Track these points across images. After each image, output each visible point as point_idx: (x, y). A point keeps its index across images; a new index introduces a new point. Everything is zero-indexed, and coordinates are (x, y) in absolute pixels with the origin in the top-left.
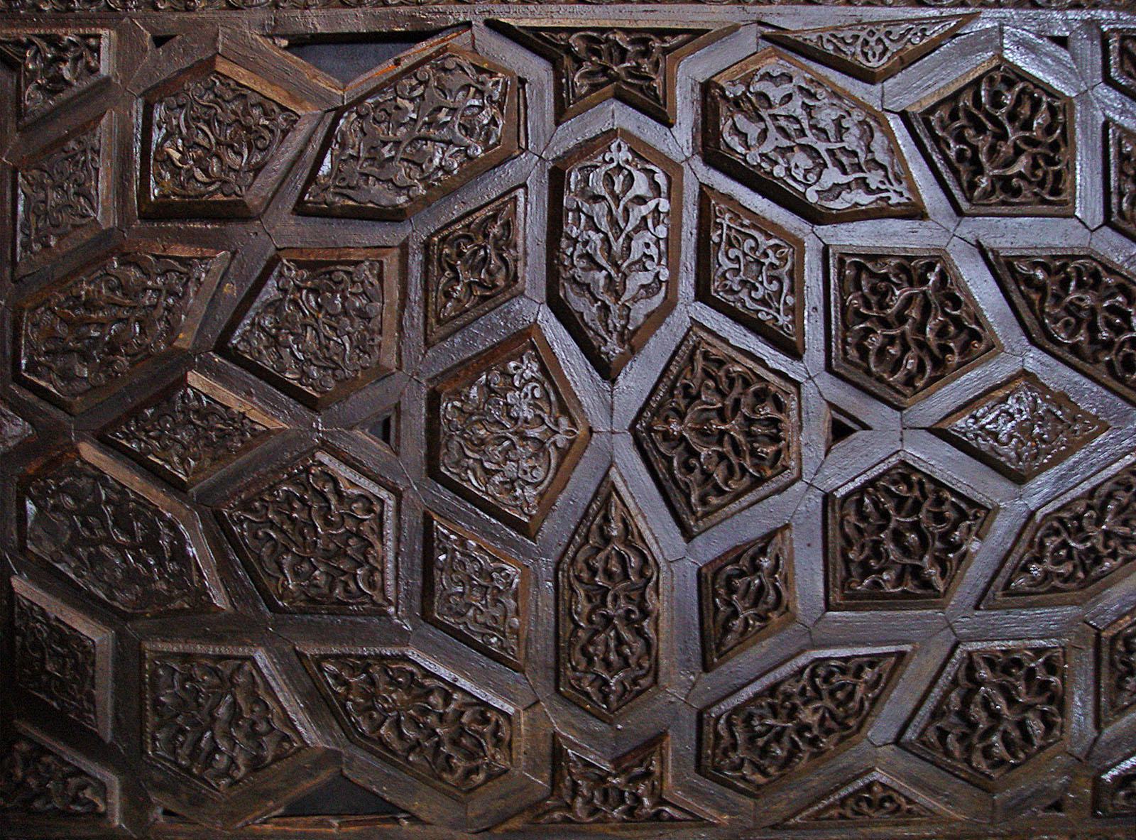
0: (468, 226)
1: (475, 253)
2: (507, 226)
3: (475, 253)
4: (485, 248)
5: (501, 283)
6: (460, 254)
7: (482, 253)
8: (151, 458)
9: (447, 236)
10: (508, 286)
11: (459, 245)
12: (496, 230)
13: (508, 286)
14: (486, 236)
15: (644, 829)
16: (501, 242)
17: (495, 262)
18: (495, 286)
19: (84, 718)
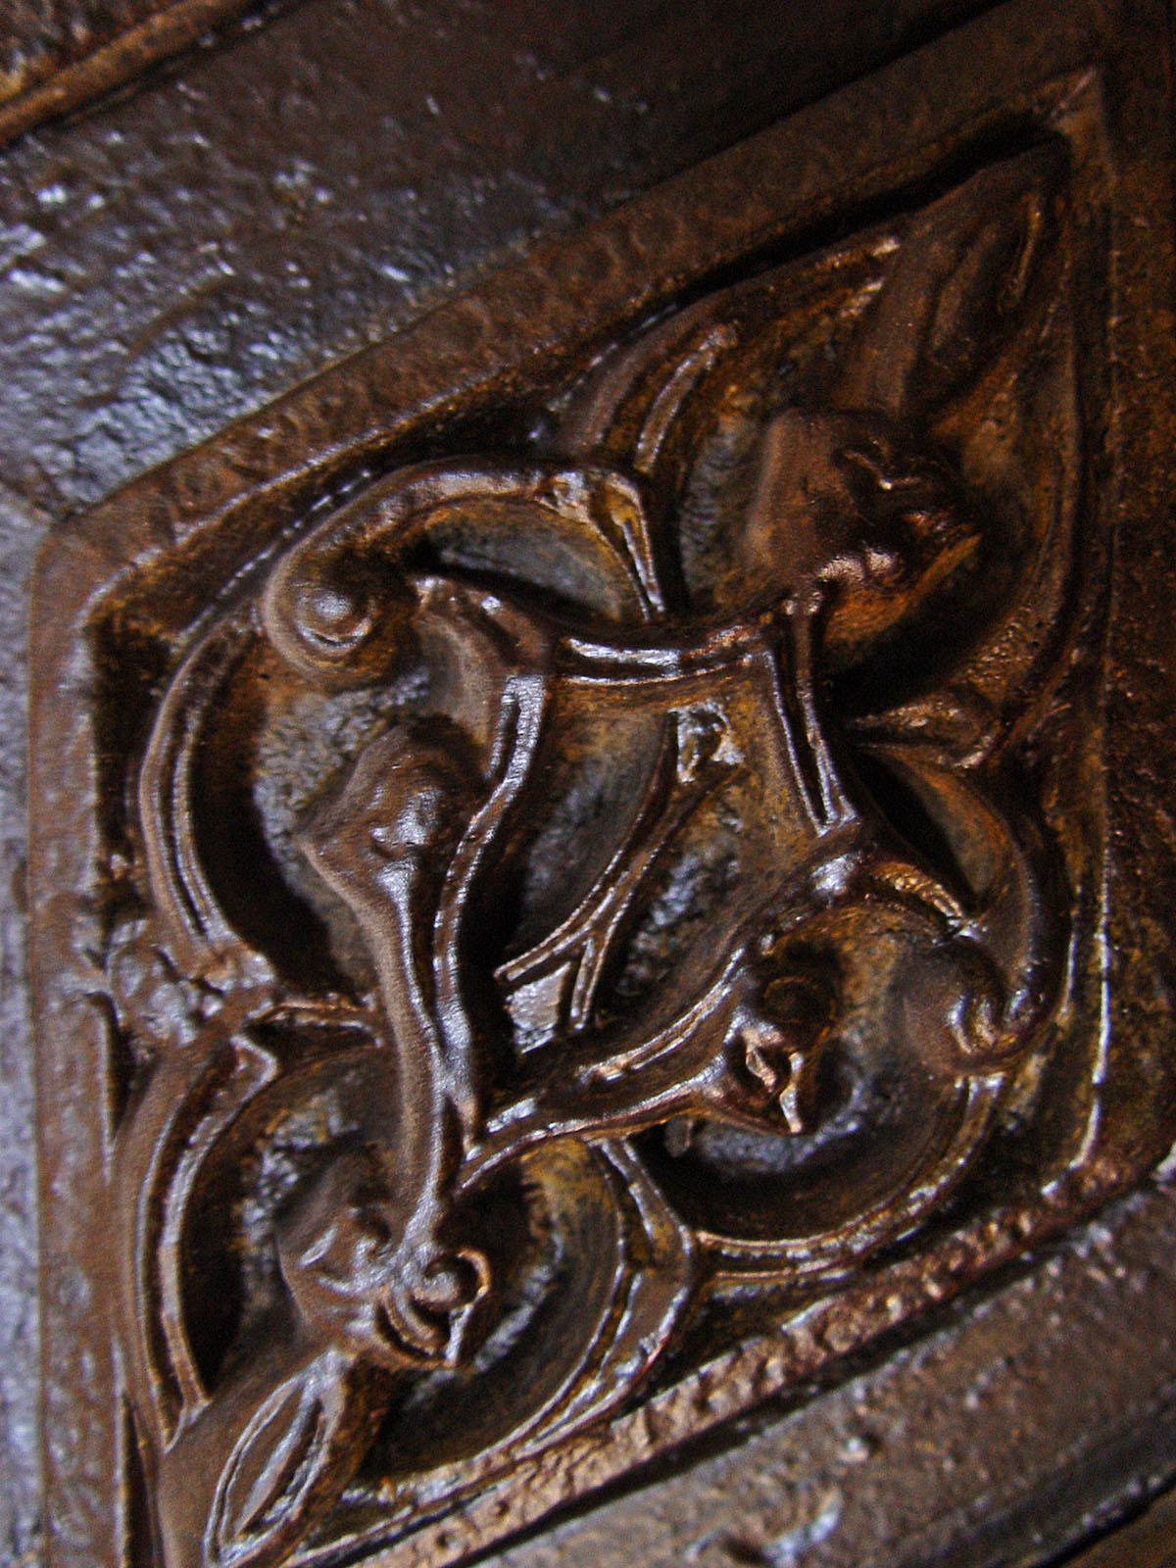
0: (706, 1333)
1: (625, 1001)
2: (231, 1328)
3: (625, 1001)
4: (498, 1068)
5: (299, 620)
6: (802, 985)
7: (533, 1007)
8: (901, 1237)
9: (967, 1202)
10: (204, 583)
11: (823, 1096)
12: (379, 1282)
13: (204, 583)
14: (489, 1217)
15: (170, 894)
16: (314, 1120)
17: (375, 908)
18: (372, 577)
19: (588, 1371)
